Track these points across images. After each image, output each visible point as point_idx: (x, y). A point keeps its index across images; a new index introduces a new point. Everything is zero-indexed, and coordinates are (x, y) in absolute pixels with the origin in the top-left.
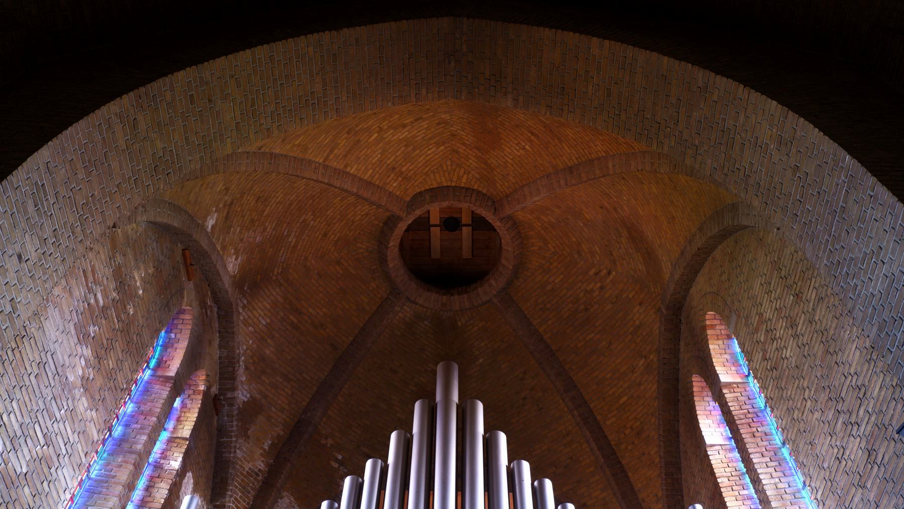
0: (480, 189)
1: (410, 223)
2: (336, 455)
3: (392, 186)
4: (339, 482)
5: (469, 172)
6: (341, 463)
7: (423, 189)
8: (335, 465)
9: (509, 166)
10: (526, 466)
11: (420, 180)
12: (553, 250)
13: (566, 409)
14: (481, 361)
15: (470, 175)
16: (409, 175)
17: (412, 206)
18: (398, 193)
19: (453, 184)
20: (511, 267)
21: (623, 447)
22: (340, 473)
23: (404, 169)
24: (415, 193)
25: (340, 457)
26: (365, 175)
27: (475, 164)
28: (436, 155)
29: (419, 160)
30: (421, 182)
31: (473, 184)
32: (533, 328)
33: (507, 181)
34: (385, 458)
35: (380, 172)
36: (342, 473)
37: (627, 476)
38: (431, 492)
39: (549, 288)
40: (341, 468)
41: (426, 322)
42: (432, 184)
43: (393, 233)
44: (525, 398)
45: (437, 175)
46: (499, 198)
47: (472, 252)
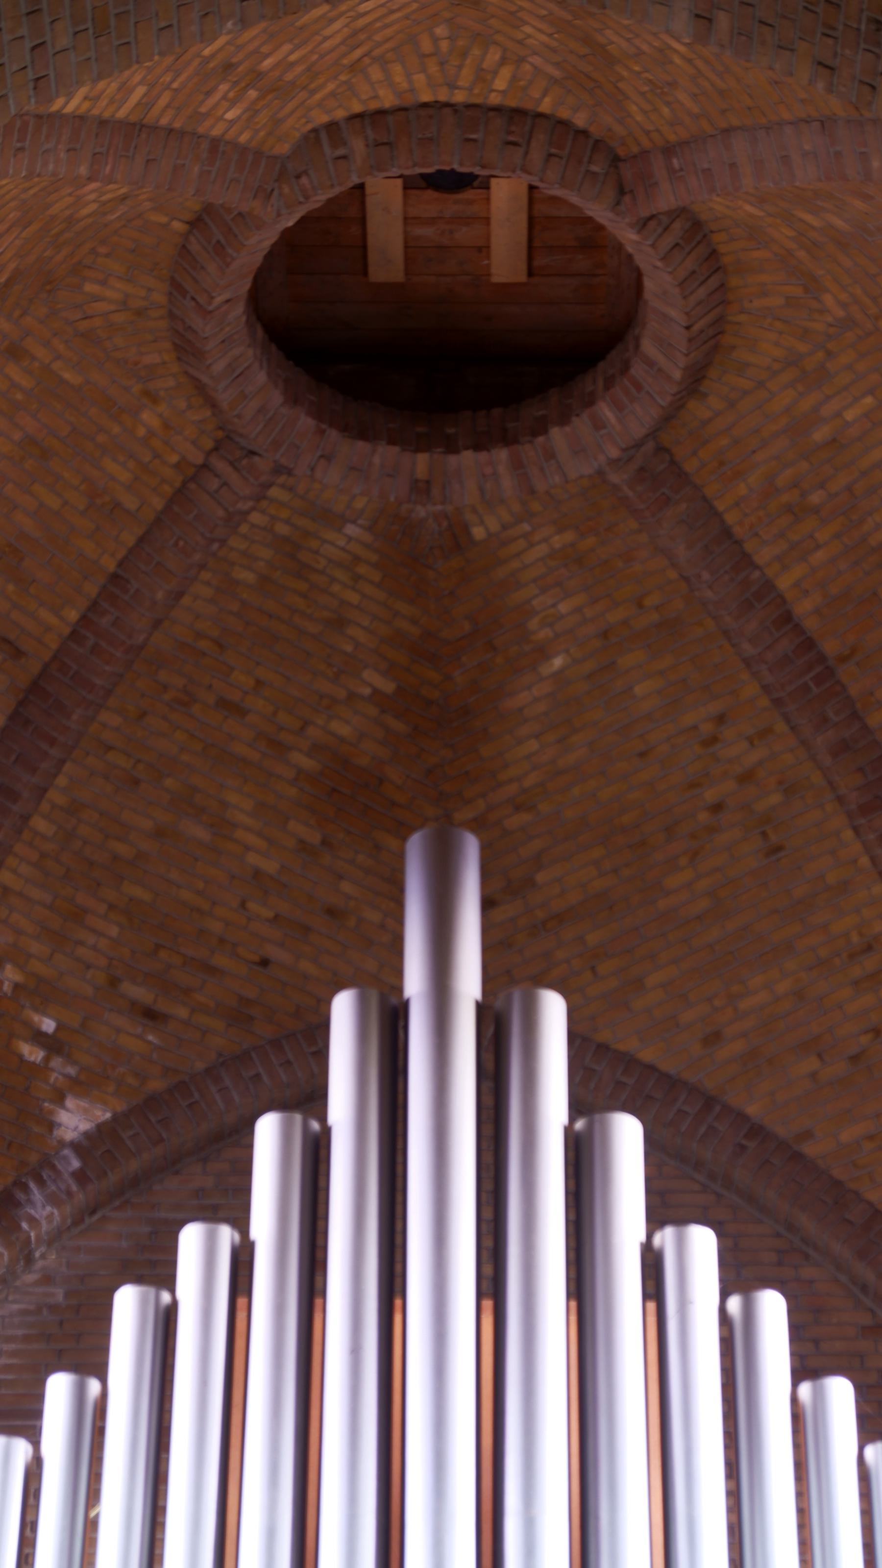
0: (564, 113)
1: (290, 224)
2: (36, 1018)
3: (221, 118)
4: (51, 1112)
5: (521, 60)
7: (340, 114)
8: (33, 1053)
9: (677, 60)
11: (331, 87)
12: (841, 313)
13: (865, 861)
14: (558, 662)
15: (527, 67)
16: (289, 77)
17: (298, 177)
18: (243, 138)
19: (459, 97)
20: (677, 375)
22: (52, 1080)
23: (268, 63)
24: (309, 127)
25: (48, 1025)
26: (119, 108)
27: (544, 38)
28: (392, 12)
29: (328, 32)
30: (333, 94)
31: (536, 94)
32: (756, 574)
33: (668, 104)
35: (175, 85)
36: (60, 1077)
38: (398, 1302)
39: (820, 435)
40: (56, 1062)
41: (351, 530)
42: (376, 97)
43: (228, 265)
44: (717, 808)
45: (397, 69)
46: (635, 150)
47: (530, 258)
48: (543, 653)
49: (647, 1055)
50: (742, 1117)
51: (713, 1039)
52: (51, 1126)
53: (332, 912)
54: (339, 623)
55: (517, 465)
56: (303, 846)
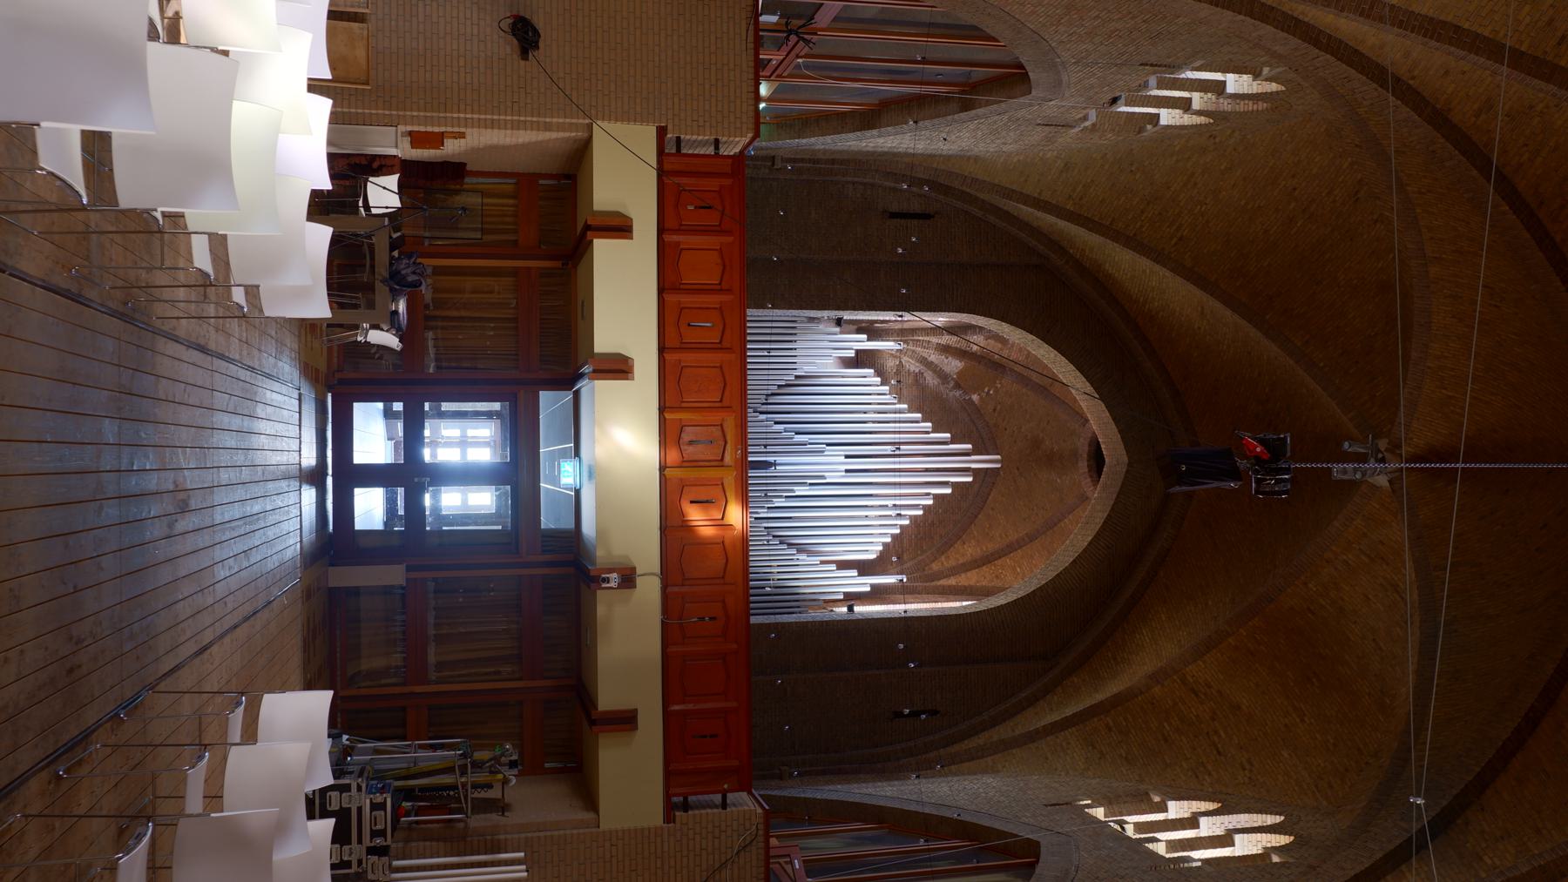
6: (988, 393)
8: (986, 390)
10: (930, 502)
21: (993, 568)
25: (991, 392)
34: (932, 432)
37: (975, 568)
48: (1060, 478)
49: (990, 498)
50: (979, 514)
51: (993, 509)
52: (974, 394)
53: (1015, 442)
54: (1064, 441)
55: (1084, 473)
56: (1027, 436)
